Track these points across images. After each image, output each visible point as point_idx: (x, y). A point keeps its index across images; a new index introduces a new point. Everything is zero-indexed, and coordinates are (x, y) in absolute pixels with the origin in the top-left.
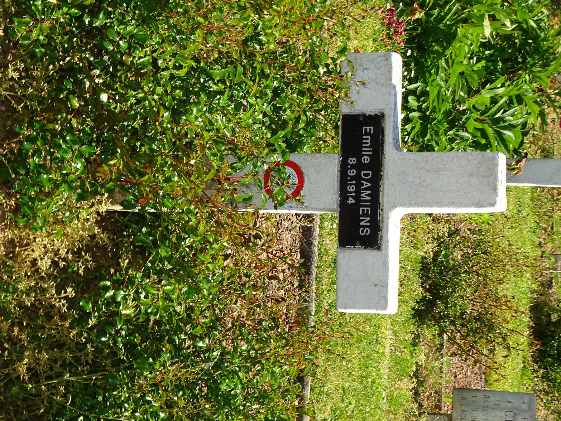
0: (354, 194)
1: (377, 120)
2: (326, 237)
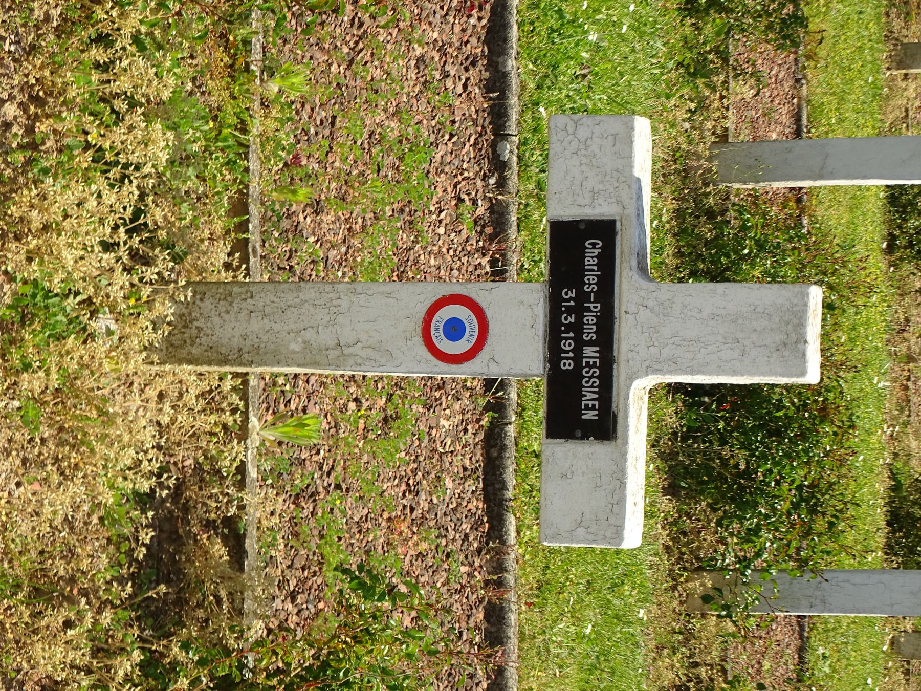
0: (571, 355)
2: (527, 427)
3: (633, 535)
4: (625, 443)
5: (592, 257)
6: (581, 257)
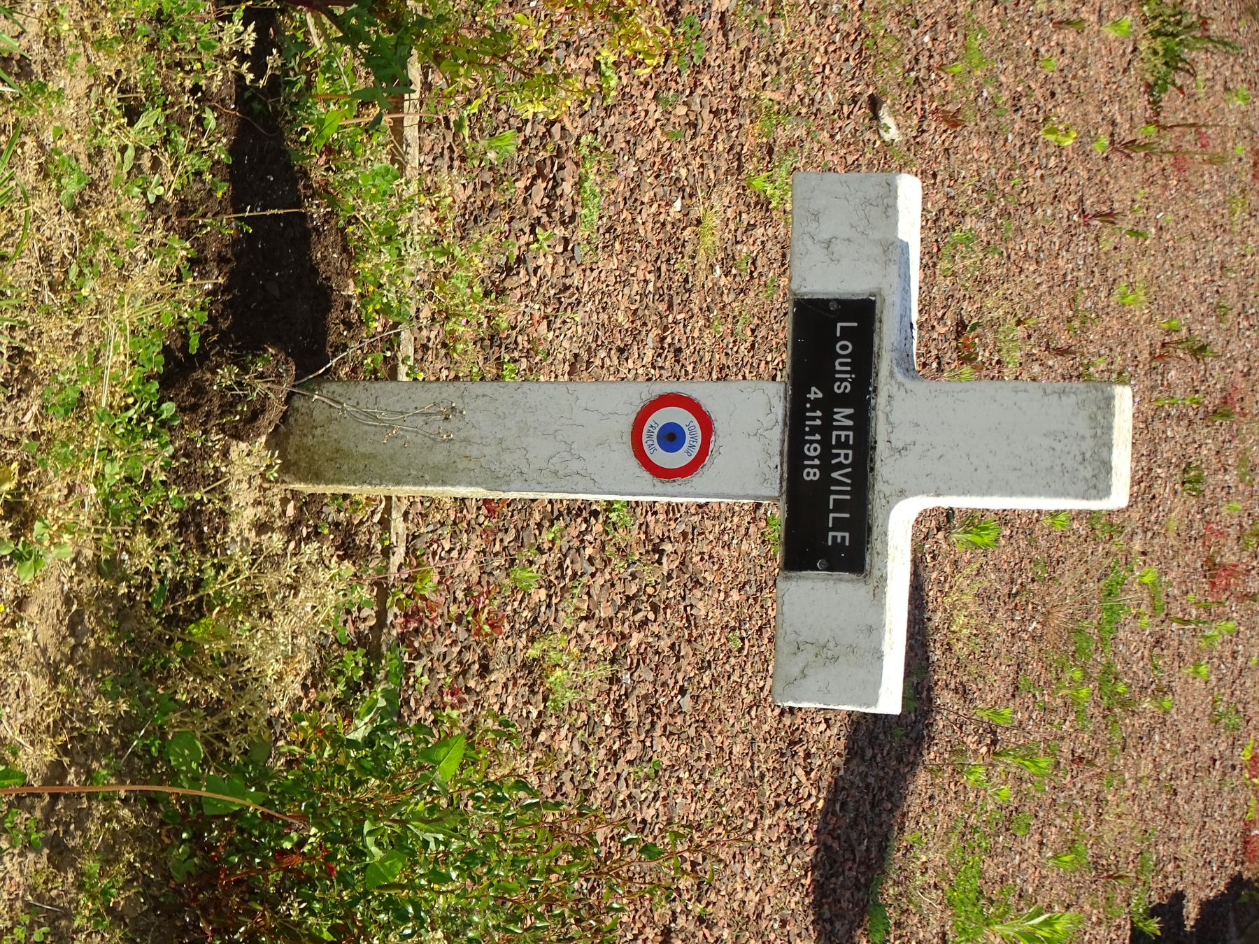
0: (817, 462)
1: (861, 314)
4: (883, 579)
6: (831, 349)
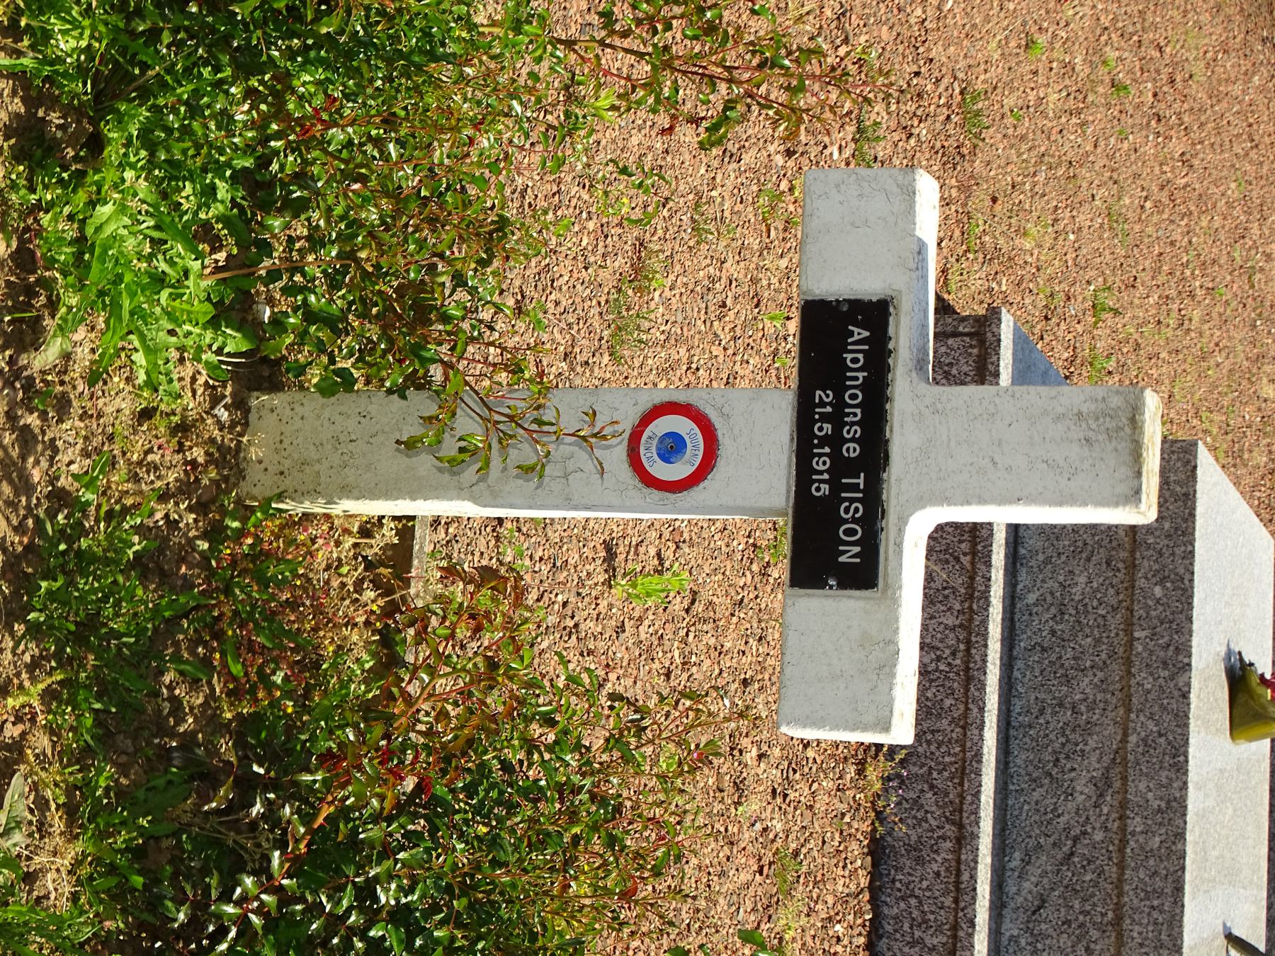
0: (826, 476)
3: (903, 732)
5: (853, 424)
